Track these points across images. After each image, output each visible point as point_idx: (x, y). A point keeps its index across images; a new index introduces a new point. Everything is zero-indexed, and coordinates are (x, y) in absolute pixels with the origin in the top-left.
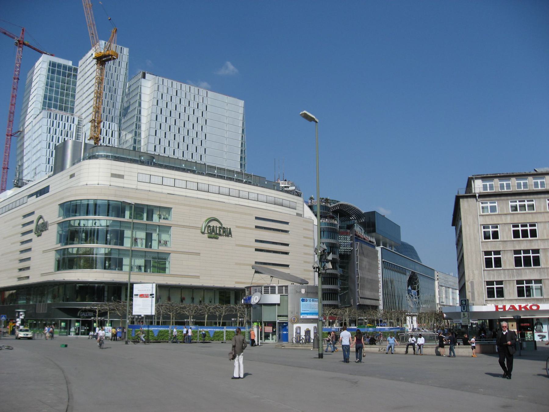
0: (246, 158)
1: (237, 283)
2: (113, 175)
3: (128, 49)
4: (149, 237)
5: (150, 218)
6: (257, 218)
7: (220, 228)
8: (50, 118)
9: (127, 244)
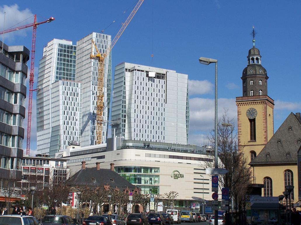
0: (189, 125)
1: (186, 197)
2: (136, 155)
3: (111, 36)
4: (151, 179)
5: (151, 171)
6: (194, 169)
7: (179, 174)
8: (64, 85)
9: (143, 183)
